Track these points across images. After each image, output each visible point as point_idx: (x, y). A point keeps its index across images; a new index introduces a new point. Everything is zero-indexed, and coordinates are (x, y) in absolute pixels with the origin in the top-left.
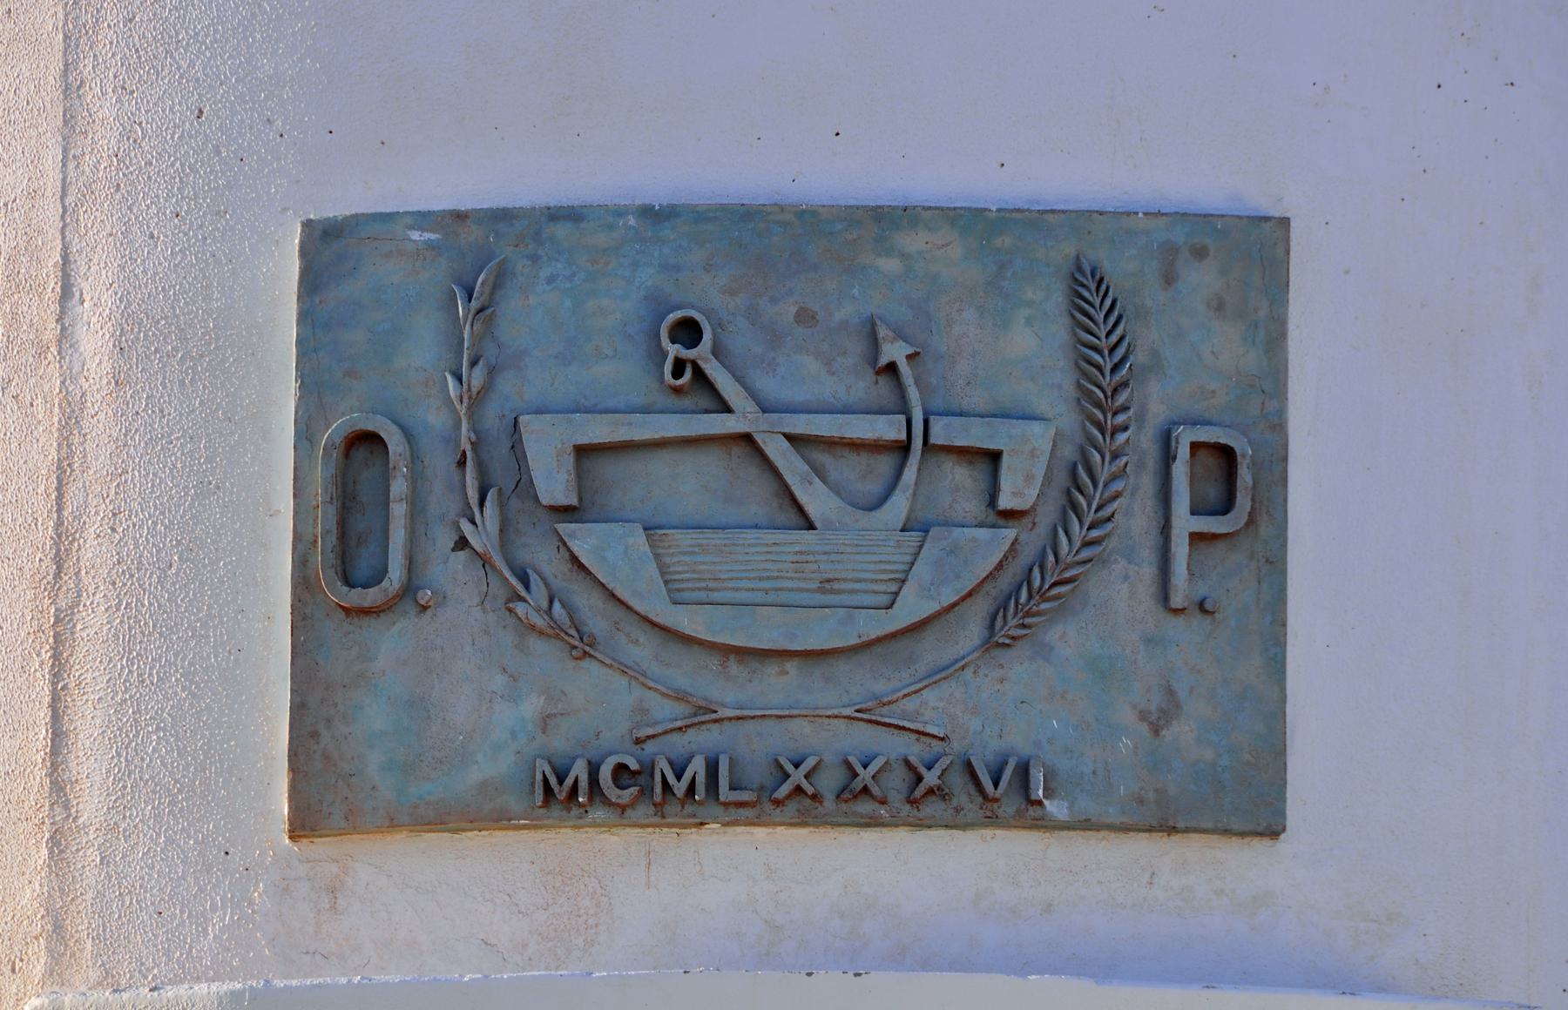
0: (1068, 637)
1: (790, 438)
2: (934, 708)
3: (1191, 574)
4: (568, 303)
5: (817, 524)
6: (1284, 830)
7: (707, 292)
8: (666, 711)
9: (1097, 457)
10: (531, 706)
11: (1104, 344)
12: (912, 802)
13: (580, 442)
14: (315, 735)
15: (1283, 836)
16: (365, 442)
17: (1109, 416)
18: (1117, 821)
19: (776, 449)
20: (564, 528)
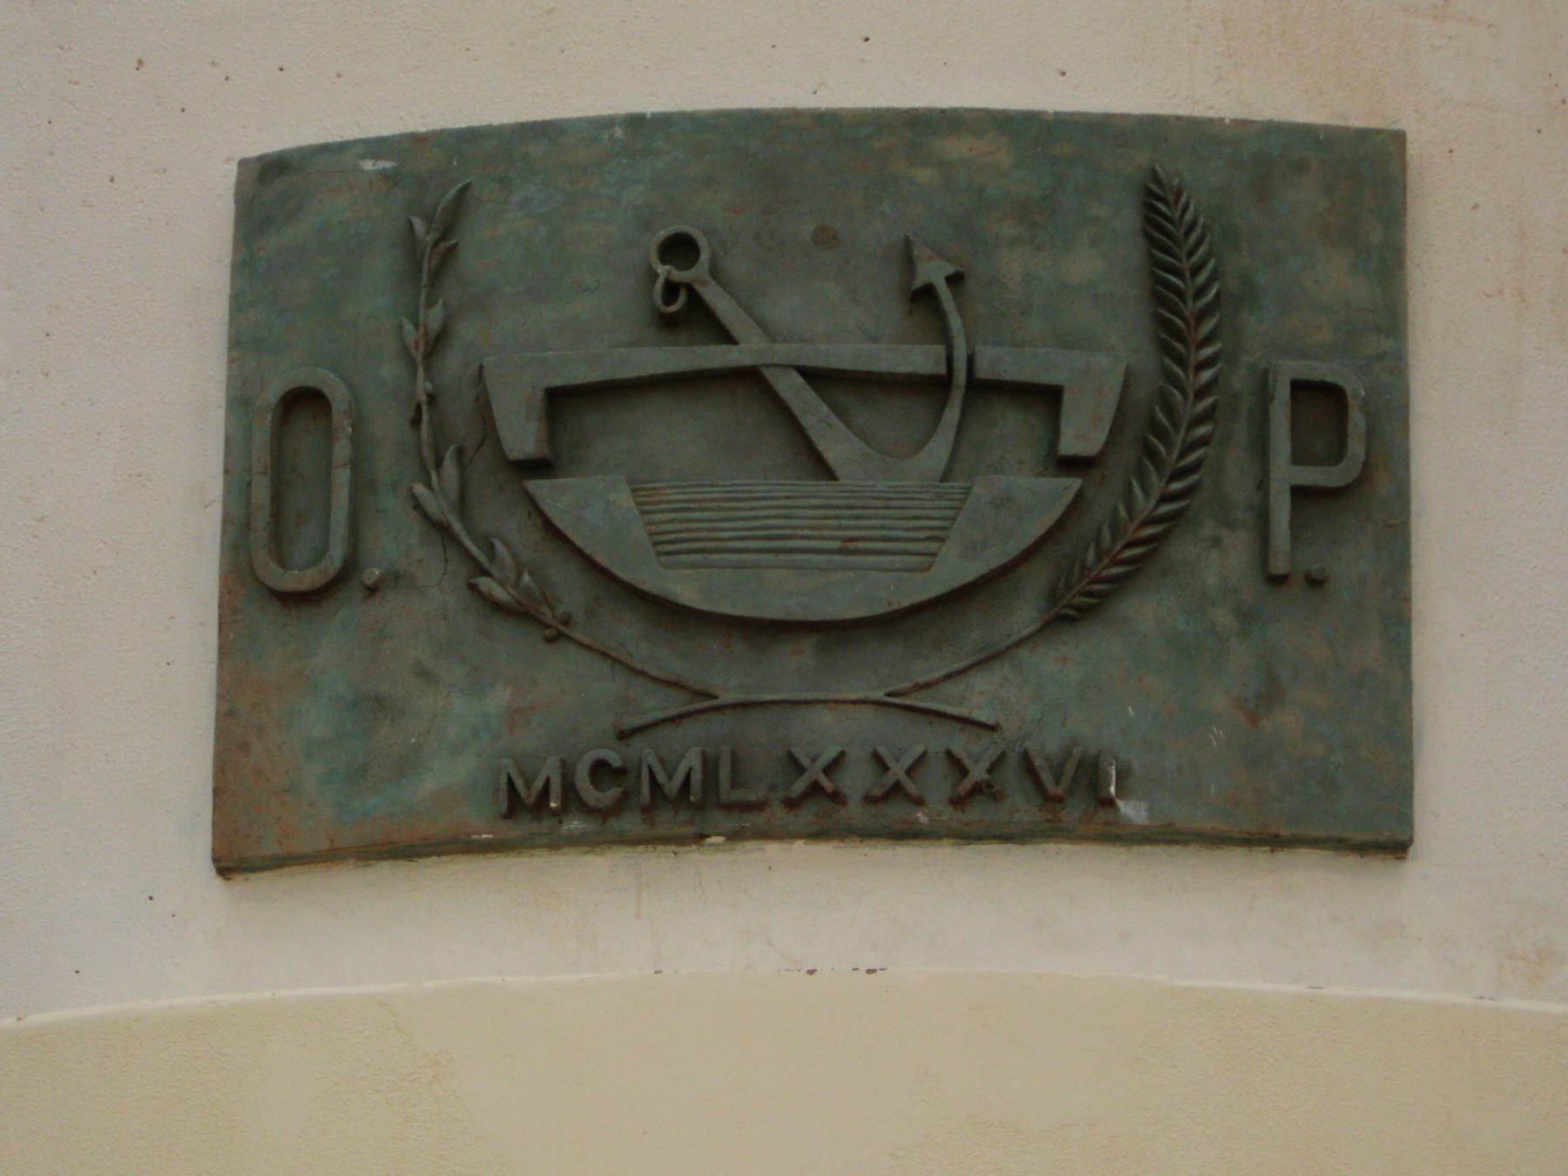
0: (1148, 610)
1: (805, 372)
2: (979, 696)
3: (1294, 539)
4: (543, 230)
5: (839, 473)
6: (1411, 841)
7: (704, 213)
8: (654, 705)
9: (1179, 397)
10: (500, 698)
11: (1186, 265)
12: (957, 802)
13: (557, 382)
14: (245, 746)
15: (1411, 850)
16: (304, 402)
17: (1191, 371)
18: (1207, 826)
19: (790, 387)
20: (537, 486)
